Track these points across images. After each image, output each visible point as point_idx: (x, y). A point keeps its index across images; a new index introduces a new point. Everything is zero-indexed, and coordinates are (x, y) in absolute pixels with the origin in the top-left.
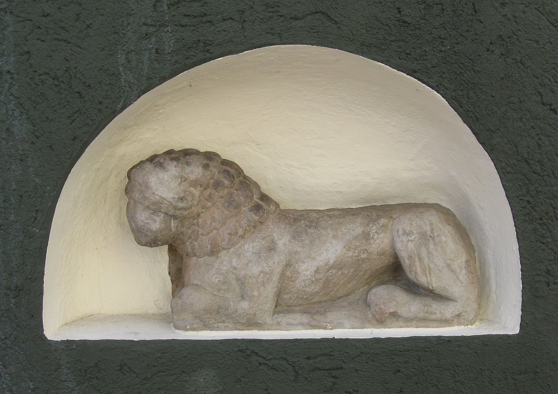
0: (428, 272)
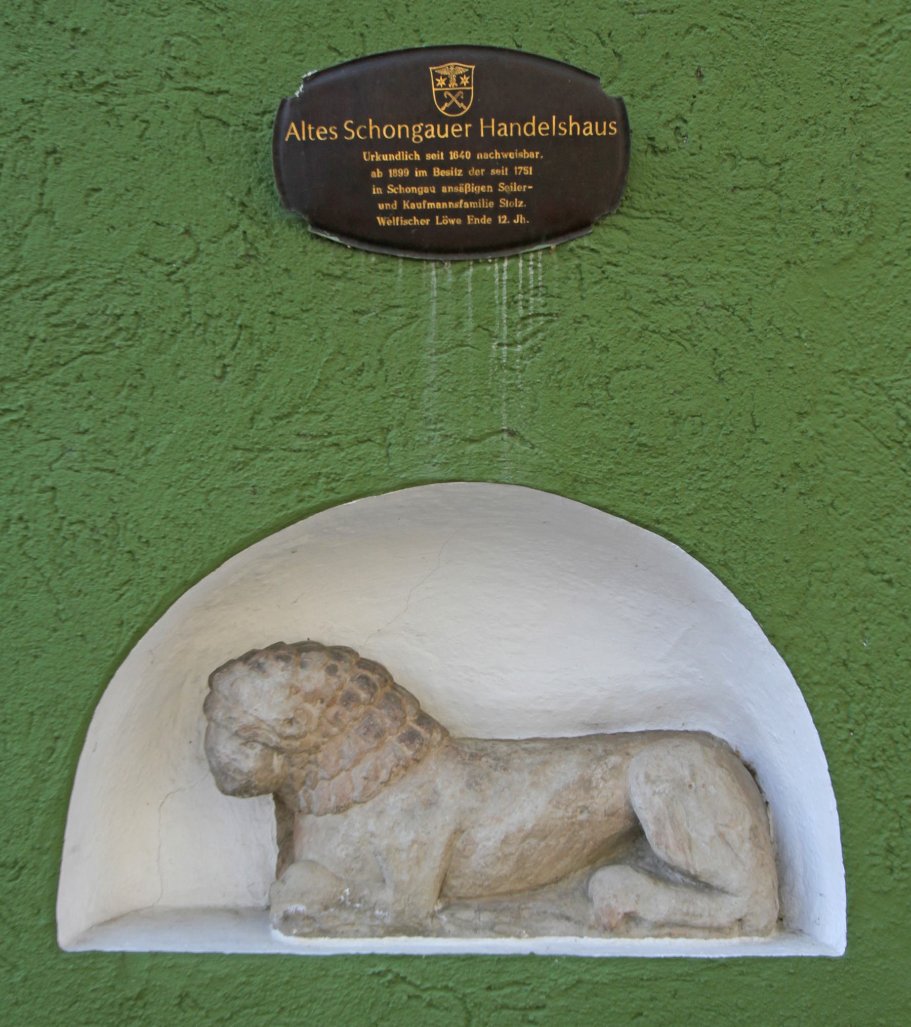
0: (686, 846)
